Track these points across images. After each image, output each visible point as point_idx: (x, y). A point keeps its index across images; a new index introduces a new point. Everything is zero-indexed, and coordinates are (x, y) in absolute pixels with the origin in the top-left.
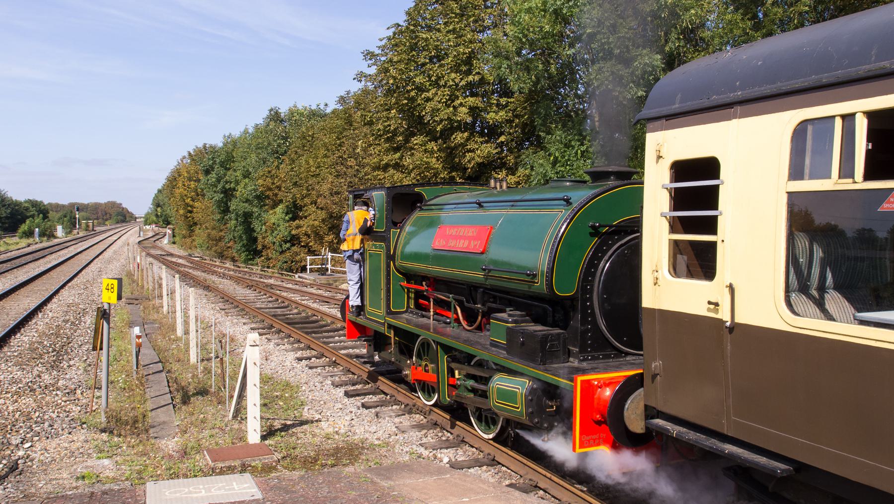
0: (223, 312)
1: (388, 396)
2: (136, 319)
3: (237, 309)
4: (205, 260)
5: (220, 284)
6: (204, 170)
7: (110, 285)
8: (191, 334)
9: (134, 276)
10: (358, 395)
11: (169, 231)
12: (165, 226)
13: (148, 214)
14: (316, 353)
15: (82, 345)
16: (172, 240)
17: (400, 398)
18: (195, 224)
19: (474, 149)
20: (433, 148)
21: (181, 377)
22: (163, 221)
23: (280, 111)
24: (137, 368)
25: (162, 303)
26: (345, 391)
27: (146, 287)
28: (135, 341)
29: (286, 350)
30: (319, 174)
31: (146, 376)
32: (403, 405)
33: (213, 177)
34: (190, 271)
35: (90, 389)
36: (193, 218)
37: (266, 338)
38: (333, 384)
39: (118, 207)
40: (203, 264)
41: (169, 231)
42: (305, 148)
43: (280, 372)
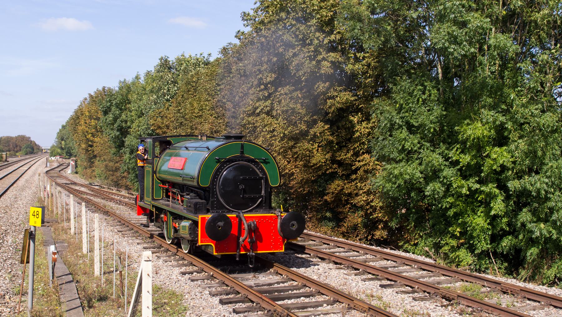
0: (120, 234)
1: (255, 304)
2: (49, 239)
3: (132, 231)
4: (104, 188)
5: (117, 209)
6: (103, 111)
7: (35, 212)
8: (95, 251)
9: (44, 202)
10: (231, 303)
11: (72, 162)
12: (68, 157)
13: (53, 146)
14: (197, 268)
15: (6, 260)
16: (75, 170)
17: (264, 305)
18: (95, 156)
19: (334, 96)
20: (298, 95)
21: (88, 286)
22: (67, 153)
23: (169, 59)
24: (53, 278)
25: (69, 226)
26: (220, 300)
27: (55, 212)
28: (50, 257)
29: (172, 266)
30: (202, 115)
31: (60, 285)
32: (266, 311)
33: (110, 117)
34: (92, 198)
35: (15, 295)
36: (93, 151)
37: (156, 256)
38: (210, 294)
39: (27, 140)
40: (102, 192)
41: (72, 163)
42: (190, 93)
43: (167, 283)
